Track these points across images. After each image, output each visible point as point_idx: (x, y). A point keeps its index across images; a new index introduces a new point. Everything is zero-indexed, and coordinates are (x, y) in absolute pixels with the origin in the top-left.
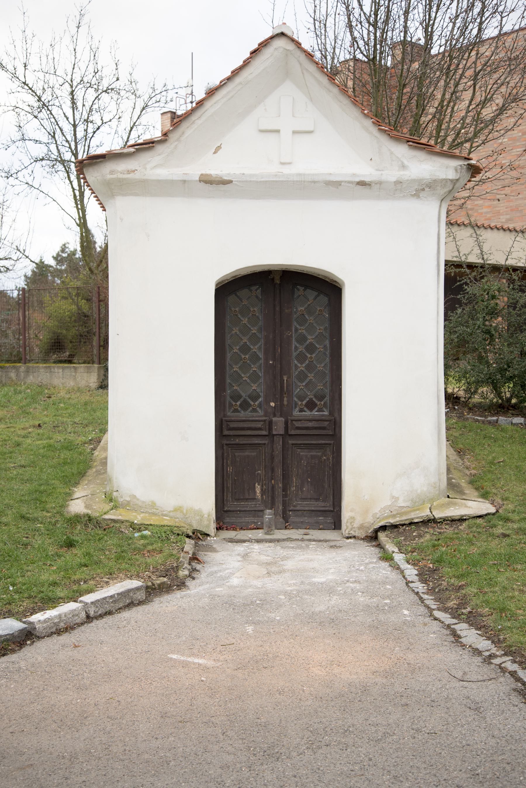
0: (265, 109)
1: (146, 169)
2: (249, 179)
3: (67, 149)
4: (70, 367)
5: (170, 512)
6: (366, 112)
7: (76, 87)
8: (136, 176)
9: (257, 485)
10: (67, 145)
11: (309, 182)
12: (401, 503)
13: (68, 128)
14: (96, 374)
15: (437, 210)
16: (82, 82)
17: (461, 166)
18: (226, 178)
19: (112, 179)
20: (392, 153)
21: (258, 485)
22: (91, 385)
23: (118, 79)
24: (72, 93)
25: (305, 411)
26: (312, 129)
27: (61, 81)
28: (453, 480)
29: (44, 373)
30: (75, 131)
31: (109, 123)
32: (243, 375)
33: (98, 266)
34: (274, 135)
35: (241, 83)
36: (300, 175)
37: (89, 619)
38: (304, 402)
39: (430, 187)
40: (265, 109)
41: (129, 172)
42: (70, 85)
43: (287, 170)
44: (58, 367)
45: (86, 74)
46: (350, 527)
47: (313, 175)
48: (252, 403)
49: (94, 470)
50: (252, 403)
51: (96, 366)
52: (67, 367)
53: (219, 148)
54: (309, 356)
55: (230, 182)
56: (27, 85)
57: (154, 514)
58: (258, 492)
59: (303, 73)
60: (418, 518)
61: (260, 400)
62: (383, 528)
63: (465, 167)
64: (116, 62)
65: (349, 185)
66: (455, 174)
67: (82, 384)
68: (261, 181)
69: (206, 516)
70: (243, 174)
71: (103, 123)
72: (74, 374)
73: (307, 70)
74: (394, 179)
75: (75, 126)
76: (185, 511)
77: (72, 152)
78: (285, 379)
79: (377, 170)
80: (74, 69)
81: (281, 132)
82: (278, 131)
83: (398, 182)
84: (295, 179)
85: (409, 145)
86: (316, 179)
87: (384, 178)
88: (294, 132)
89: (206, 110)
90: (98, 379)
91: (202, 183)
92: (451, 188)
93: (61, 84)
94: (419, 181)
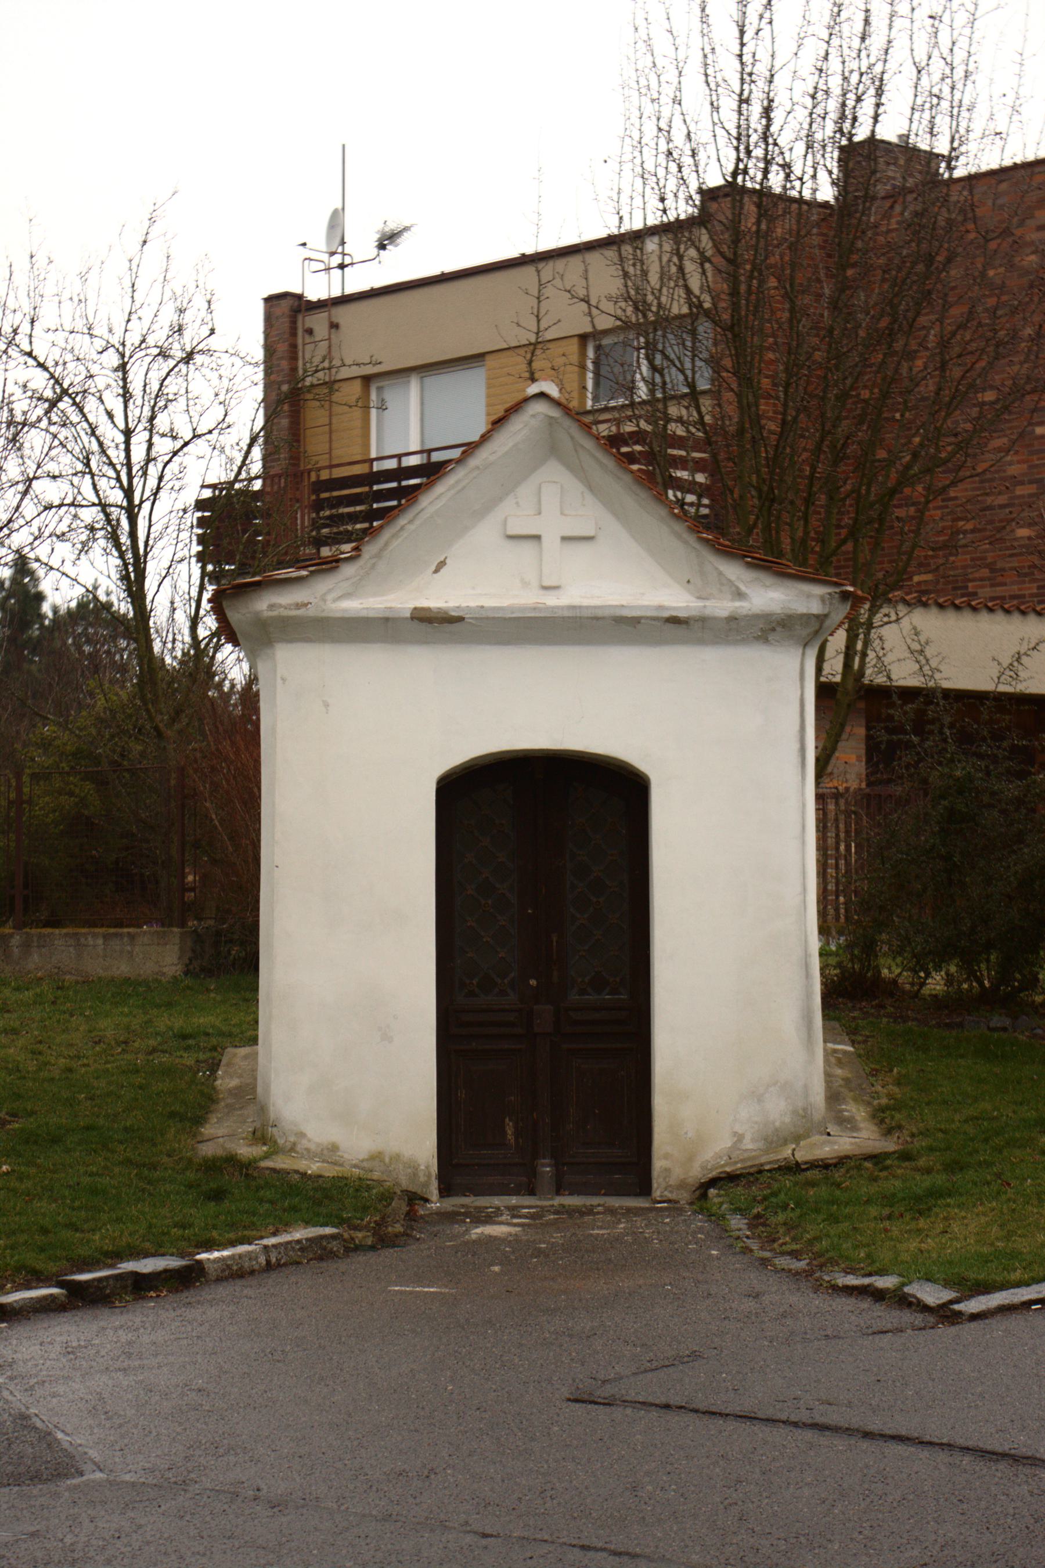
0: (517, 503)
1: (325, 601)
2: (491, 615)
3: (113, 482)
4: (121, 935)
5: (362, 1161)
6: (676, 511)
7: (131, 357)
8: (311, 612)
9: (507, 1120)
10: (112, 473)
11: (588, 618)
12: (748, 1144)
13: (112, 435)
14: (176, 948)
15: (799, 660)
16: (143, 346)
17: (830, 594)
18: (453, 614)
19: (271, 617)
20: (720, 573)
21: (510, 1120)
22: (165, 970)
23: (212, 331)
24: (123, 368)
25: (589, 994)
26: (591, 533)
27: (99, 344)
28: (846, 1114)
29: (63, 948)
30: (127, 443)
31: (208, 437)
32: (483, 934)
33: (173, 720)
34: (528, 547)
35: (478, 468)
36: (574, 607)
37: (269, 1267)
38: (587, 980)
39: (784, 626)
40: (517, 503)
41: (298, 606)
42: (120, 353)
43: (552, 600)
44: (95, 936)
45: (153, 327)
46: (664, 1185)
47: (595, 607)
48: (499, 981)
49: (223, 1104)
50: (499, 981)
51: (176, 930)
52: (116, 935)
53: (442, 564)
54: (595, 900)
55: (461, 619)
56: (35, 358)
57: (335, 1163)
58: (509, 1132)
59: (576, 451)
60: (770, 1163)
61: (512, 975)
62: (713, 1182)
63: (837, 596)
64: (209, 297)
65: (653, 622)
66: (821, 606)
67: (147, 969)
68: (510, 618)
69: (422, 1167)
70: (482, 607)
71: (194, 437)
72: (129, 948)
73: (582, 446)
74: (725, 614)
75: (128, 433)
76: (387, 1160)
77: (122, 487)
78: (555, 939)
79: (699, 598)
80: (129, 321)
81: (544, 539)
82: (537, 538)
83: (732, 619)
84: (566, 614)
85: (748, 563)
86: (600, 613)
87: (708, 612)
88: (565, 539)
89: (423, 510)
90: (179, 958)
91: (416, 621)
92: (817, 628)
93: (100, 350)
94: (766, 617)
